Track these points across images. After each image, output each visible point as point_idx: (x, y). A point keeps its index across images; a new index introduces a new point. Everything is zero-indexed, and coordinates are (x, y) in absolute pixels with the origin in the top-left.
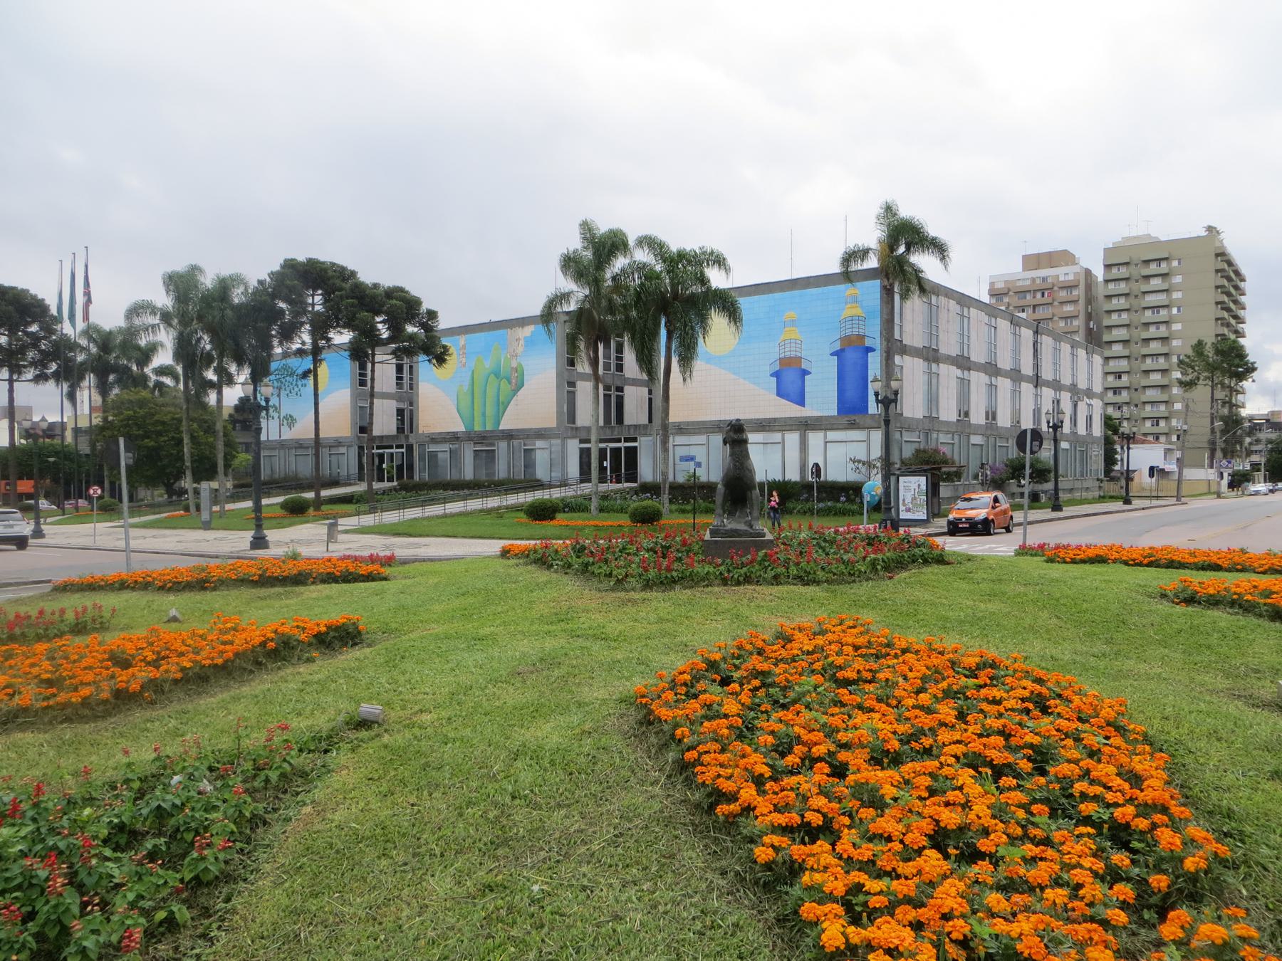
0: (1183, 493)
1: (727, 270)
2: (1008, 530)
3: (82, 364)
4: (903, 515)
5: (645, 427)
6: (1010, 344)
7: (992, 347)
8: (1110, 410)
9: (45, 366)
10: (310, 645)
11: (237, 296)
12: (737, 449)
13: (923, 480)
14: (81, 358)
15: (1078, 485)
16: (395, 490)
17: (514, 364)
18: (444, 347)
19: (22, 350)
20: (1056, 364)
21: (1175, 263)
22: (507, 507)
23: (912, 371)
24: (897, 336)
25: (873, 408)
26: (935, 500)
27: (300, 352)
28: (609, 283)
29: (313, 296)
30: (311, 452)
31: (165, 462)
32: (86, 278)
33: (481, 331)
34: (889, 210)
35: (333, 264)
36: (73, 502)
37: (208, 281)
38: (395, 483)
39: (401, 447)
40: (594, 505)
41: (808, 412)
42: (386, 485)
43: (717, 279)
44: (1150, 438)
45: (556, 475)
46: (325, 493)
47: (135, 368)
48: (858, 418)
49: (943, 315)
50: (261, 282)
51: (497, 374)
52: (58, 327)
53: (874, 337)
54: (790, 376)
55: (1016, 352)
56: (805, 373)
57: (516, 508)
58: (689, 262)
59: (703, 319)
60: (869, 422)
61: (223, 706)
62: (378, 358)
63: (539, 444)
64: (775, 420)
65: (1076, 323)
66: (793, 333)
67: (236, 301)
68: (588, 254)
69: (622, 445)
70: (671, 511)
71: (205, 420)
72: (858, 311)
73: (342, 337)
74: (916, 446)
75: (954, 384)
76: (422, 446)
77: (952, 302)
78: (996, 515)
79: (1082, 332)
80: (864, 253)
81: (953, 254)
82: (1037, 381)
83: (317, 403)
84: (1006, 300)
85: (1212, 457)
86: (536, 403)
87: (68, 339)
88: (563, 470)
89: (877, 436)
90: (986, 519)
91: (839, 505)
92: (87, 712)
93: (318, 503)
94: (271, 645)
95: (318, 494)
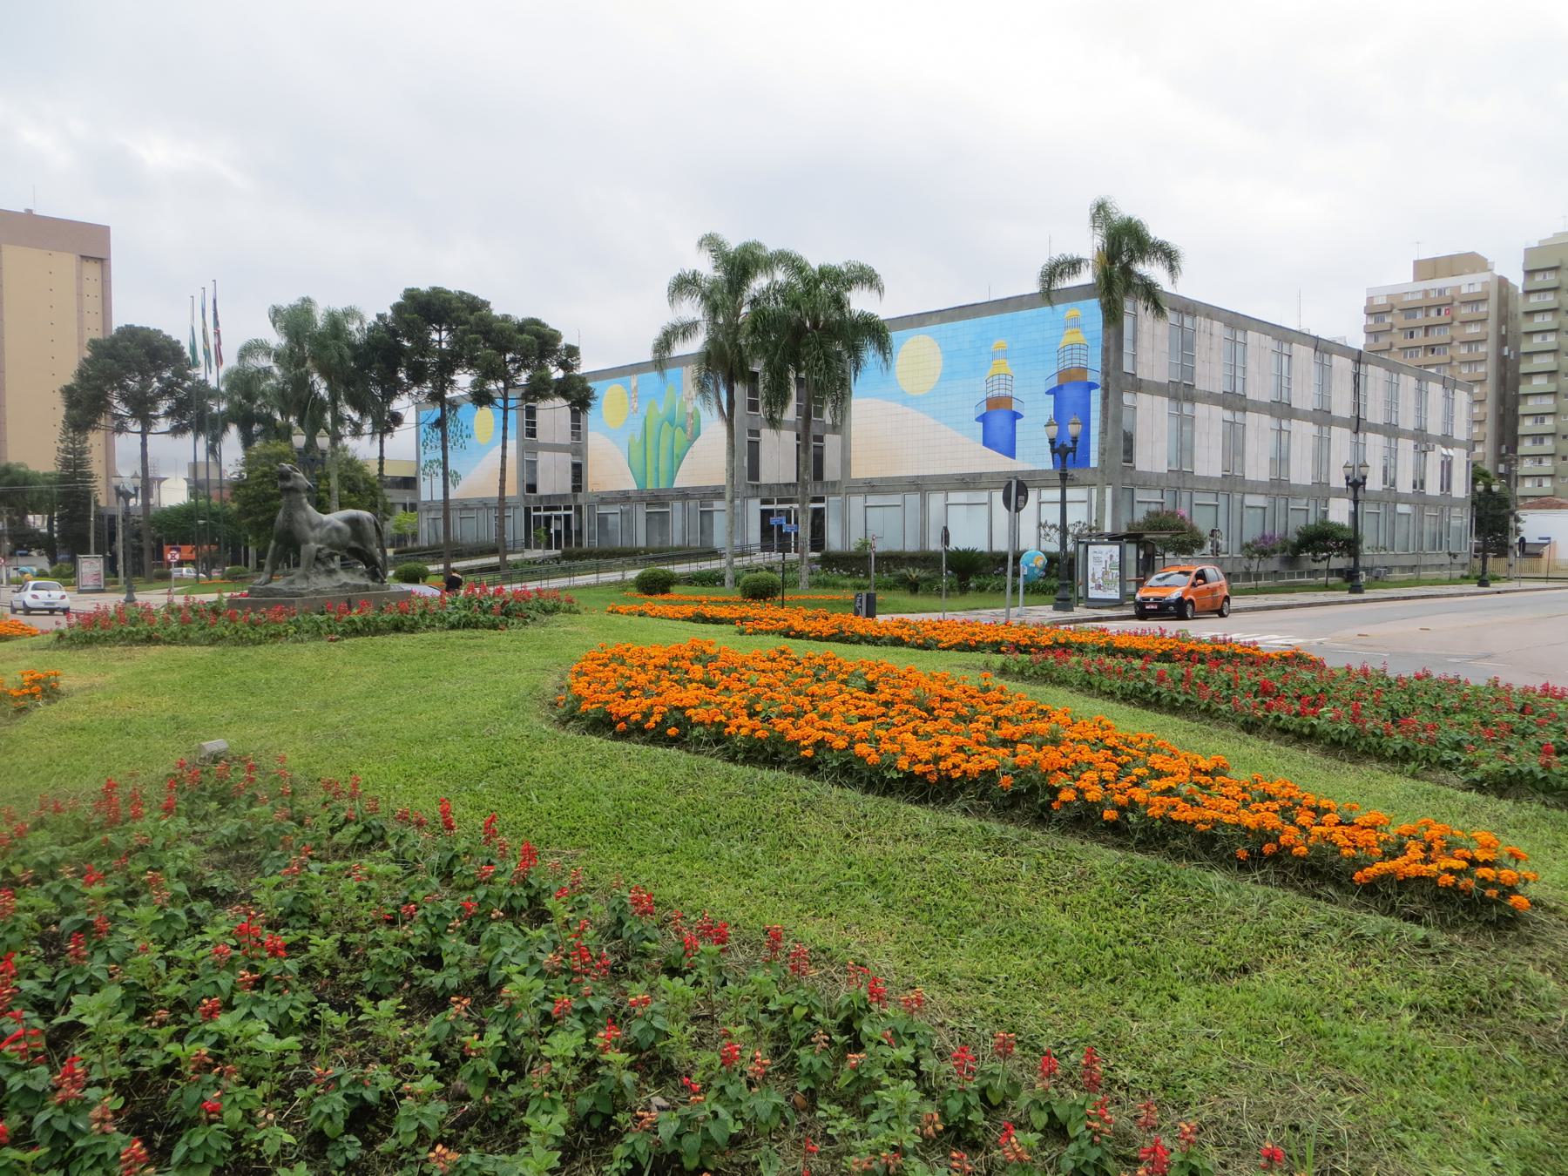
1: (881, 291)
4: (1093, 594)
7: (1284, 380)
15: (1426, 561)
16: (556, 559)
19: (153, 401)
20: (1421, 409)
24: (1127, 368)
29: (440, 331)
30: (440, 514)
35: (462, 293)
39: (568, 508)
43: (860, 302)
46: (495, 560)
47: (278, 417)
49: (1201, 342)
50: (380, 317)
53: (1095, 362)
54: (999, 420)
56: (1016, 416)
59: (855, 351)
60: (1090, 478)
61: (986, 843)
64: (981, 475)
65: (1482, 349)
66: (1003, 366)
72: (1080, 338)
74: (1153, 508)
75: (1218, 429)
76: (591, 507)
77: (1217, 325)
80: (1074, 265)
81: (1185, 264)
82: (1357, 425)
83: (473, 457)
84: (1388, 320)
86: (707, 459)
90: (1180, 600)
95: (503, 559)
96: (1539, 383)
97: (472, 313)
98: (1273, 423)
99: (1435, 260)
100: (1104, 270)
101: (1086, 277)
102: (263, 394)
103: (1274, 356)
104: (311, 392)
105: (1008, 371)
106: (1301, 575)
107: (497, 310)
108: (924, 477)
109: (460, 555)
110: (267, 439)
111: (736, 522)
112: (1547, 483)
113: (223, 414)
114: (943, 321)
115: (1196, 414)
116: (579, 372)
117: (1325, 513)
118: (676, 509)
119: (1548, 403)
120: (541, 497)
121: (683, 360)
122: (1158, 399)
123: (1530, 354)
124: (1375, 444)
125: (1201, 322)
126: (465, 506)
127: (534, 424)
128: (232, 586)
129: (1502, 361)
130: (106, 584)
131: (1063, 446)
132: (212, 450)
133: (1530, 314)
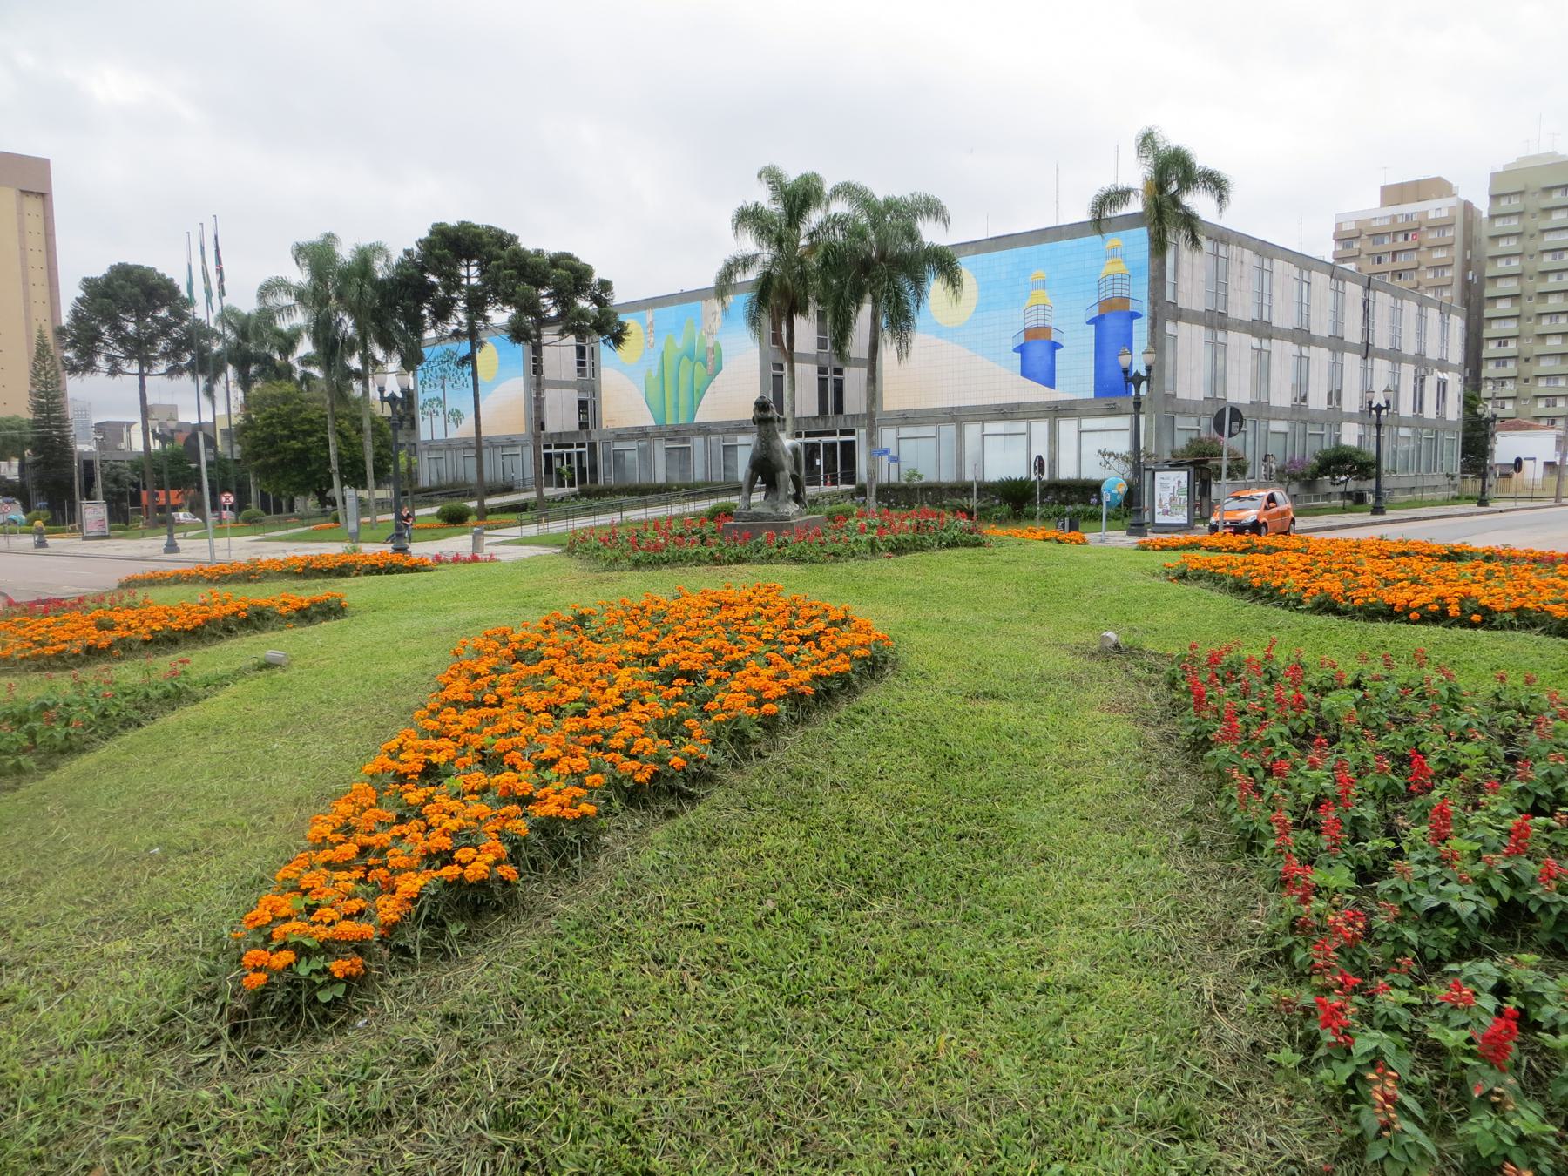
1: (947, 222)
3: (219, 354)
4: (1160, 519)
7: (1304, 308)
9: (178, 357)
10: (290, 618)
11: (381, 270)
14: (217, 347)
16: (574, 495)
17: (710, 345)
18: (622, 324)
19: (152, 340)
20: (1421, 333)
23: (1189, 340)
24: (1169, 297)
26: (1205, 501)
27: (456, 334)
29: (468, 266)
30: (473, 453)
31: (315, 466)
32: (217, 251)
33: (672, 303)
35: (490, 228)
37: (345, 253)
38: (575, 489)
39: (581, 445)
41: (1059, 394)
43: (931, 233)
44: (1544, 423)
46: (490, 502)
47: (277, 357)
49: (1234, 269)
50: (408, 253)
51: (690, 355)
52: (190, 311)
53: (1140, 297)
54: (1038, 350)
56: (1055, 346)
59: (918, 283)
62: (545, 340)
64: (1019, 405)
65: (1448, 274)
66: (1042, 297)
67: (380, 276)
69: (838, 439)
71: (351, 412)
72: (1121, 268)
73: (500, 316)
74: (1194, 435)
75: (1247, 355)
78: (1269, 517)
79: (1457, 285)
80: (1122, 195)
81: (1235, 195)
82: (1367, 351)
83: (484, 393)
84: (1356, 246)
87: (202, 326)
92: (59, 663)
93: (483, 513)
94: (243, 615)
95: (481, 503)
96: (1503, 307)
98: (1294, 349)
100: (1155, 199)
101: (1136, 206)
103: (1296, 284)
105: (1047, 301)
106: (1316, 498)
107: (528, 244)
108: (959, 408)
109: (492, 492)
110: (268, 379)
112: (1509, 405)
114: (978, 252)
117: (1338, 437)
119: (1511, 327)
122: (1196, 327)
123: (1494, 278)
124: (1381, 366)
125: (1234, 250)
128: (250, 529)
129: (1467, 285)
130: (111, 529)
133: (1495, 238)
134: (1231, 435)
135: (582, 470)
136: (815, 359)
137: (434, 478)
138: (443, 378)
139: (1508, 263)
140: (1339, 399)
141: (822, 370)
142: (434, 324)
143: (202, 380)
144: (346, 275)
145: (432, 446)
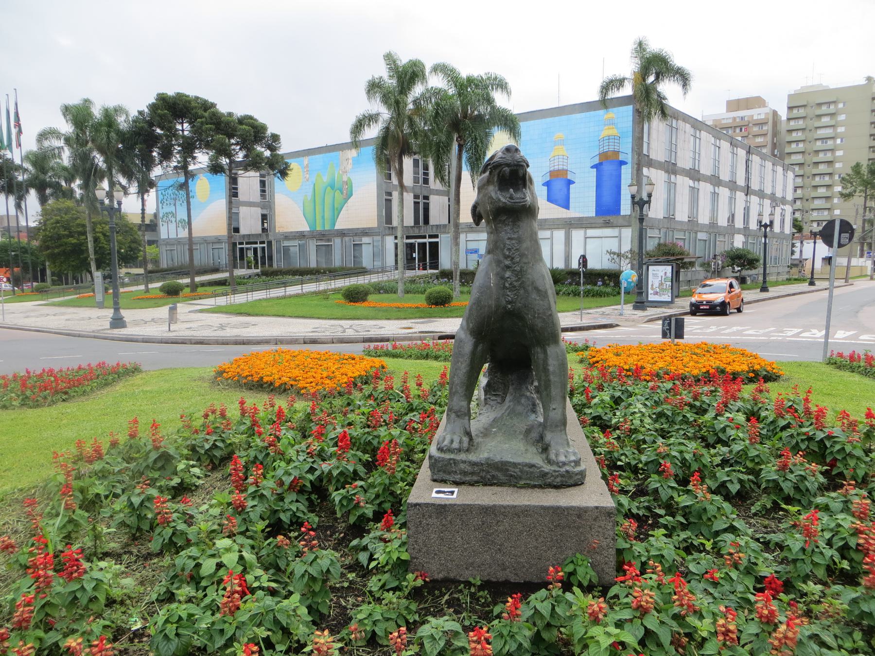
0: (850, 276)
1: (509, 93)
2: (739, 310)
4: (651, 298)
5: (445, 226)
6: (728, 161)
8: (798, 215)
12: (506, 232)
13: (669, 269)
16: (258, 275)
17: (345, 179)
18: (286, 164)
21: (841, 106)
22: (332, 290)
24: (645, 152)
25: (626, 208)
28: (411, 106)
29: (182, 123)
33: (320, 153)
34: (641, 46)
35: (197, 98)
36: (29, 284)
37: (97, 112)
38: (259, 271)
39: (263, 242)
40: (400, 287)
41: (574, 213)
42: (250, 272)
43: (500, 100)
45: (378, 264)
46: (198, 279)
47: (63, 184)
48: (612, 219)
51: (332, 187)
54: (558, 185)
55: (734, 167)
56: (570, 182)
57: (336, 291)
58: (477, 86)
60: (620, 221)
63: (365, 240)
66: (561, 151)
68: (394, 82)
69: (427, 240)
70: (462, 292)
72: (614, 132)
75: (687, 191)
77: (688, 126)
81: (694, 84)
82: (748, 191)
83: (199, 206)
85: (862, 250)
88: (383, 259)
89: (628, 234)
91: (596, 288)
95: (193, 280)
97: (205, 110)
99: (747, 99)
101: (627, 90)
102: (52, 169)
104: (92, 164)
105: (565, 153)
110: (57, 198)
111: (378, 254)
113: (26, 181)
115: (677, 183)
116: (281, 152)
118: (337, 242)
120: (244, 236)
121: (367, 142)
123: (790, 154)
126: (205, 241)
127: (236, 189)
128: (40, 296)
131: (641, 199)
132: (18, 206)
133: (790, 131)
134: (840, 245)
135: (263, 257)
136: (413, 189)
137: (170, 262)
138: (175, 200)
139: (797, 145)
140: (733, 221)
141: (416, 197)
142: (161, 162)
143: (12, 200)
144: (97, 127)
145: (168, 242)
